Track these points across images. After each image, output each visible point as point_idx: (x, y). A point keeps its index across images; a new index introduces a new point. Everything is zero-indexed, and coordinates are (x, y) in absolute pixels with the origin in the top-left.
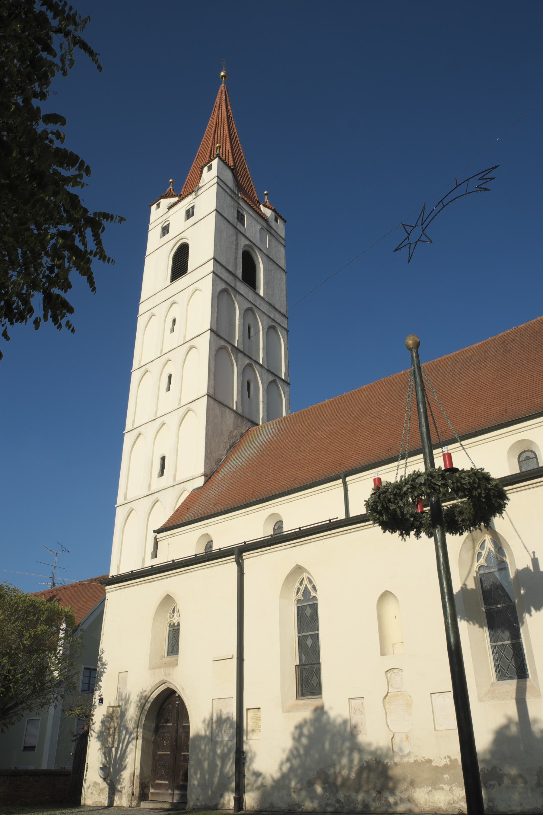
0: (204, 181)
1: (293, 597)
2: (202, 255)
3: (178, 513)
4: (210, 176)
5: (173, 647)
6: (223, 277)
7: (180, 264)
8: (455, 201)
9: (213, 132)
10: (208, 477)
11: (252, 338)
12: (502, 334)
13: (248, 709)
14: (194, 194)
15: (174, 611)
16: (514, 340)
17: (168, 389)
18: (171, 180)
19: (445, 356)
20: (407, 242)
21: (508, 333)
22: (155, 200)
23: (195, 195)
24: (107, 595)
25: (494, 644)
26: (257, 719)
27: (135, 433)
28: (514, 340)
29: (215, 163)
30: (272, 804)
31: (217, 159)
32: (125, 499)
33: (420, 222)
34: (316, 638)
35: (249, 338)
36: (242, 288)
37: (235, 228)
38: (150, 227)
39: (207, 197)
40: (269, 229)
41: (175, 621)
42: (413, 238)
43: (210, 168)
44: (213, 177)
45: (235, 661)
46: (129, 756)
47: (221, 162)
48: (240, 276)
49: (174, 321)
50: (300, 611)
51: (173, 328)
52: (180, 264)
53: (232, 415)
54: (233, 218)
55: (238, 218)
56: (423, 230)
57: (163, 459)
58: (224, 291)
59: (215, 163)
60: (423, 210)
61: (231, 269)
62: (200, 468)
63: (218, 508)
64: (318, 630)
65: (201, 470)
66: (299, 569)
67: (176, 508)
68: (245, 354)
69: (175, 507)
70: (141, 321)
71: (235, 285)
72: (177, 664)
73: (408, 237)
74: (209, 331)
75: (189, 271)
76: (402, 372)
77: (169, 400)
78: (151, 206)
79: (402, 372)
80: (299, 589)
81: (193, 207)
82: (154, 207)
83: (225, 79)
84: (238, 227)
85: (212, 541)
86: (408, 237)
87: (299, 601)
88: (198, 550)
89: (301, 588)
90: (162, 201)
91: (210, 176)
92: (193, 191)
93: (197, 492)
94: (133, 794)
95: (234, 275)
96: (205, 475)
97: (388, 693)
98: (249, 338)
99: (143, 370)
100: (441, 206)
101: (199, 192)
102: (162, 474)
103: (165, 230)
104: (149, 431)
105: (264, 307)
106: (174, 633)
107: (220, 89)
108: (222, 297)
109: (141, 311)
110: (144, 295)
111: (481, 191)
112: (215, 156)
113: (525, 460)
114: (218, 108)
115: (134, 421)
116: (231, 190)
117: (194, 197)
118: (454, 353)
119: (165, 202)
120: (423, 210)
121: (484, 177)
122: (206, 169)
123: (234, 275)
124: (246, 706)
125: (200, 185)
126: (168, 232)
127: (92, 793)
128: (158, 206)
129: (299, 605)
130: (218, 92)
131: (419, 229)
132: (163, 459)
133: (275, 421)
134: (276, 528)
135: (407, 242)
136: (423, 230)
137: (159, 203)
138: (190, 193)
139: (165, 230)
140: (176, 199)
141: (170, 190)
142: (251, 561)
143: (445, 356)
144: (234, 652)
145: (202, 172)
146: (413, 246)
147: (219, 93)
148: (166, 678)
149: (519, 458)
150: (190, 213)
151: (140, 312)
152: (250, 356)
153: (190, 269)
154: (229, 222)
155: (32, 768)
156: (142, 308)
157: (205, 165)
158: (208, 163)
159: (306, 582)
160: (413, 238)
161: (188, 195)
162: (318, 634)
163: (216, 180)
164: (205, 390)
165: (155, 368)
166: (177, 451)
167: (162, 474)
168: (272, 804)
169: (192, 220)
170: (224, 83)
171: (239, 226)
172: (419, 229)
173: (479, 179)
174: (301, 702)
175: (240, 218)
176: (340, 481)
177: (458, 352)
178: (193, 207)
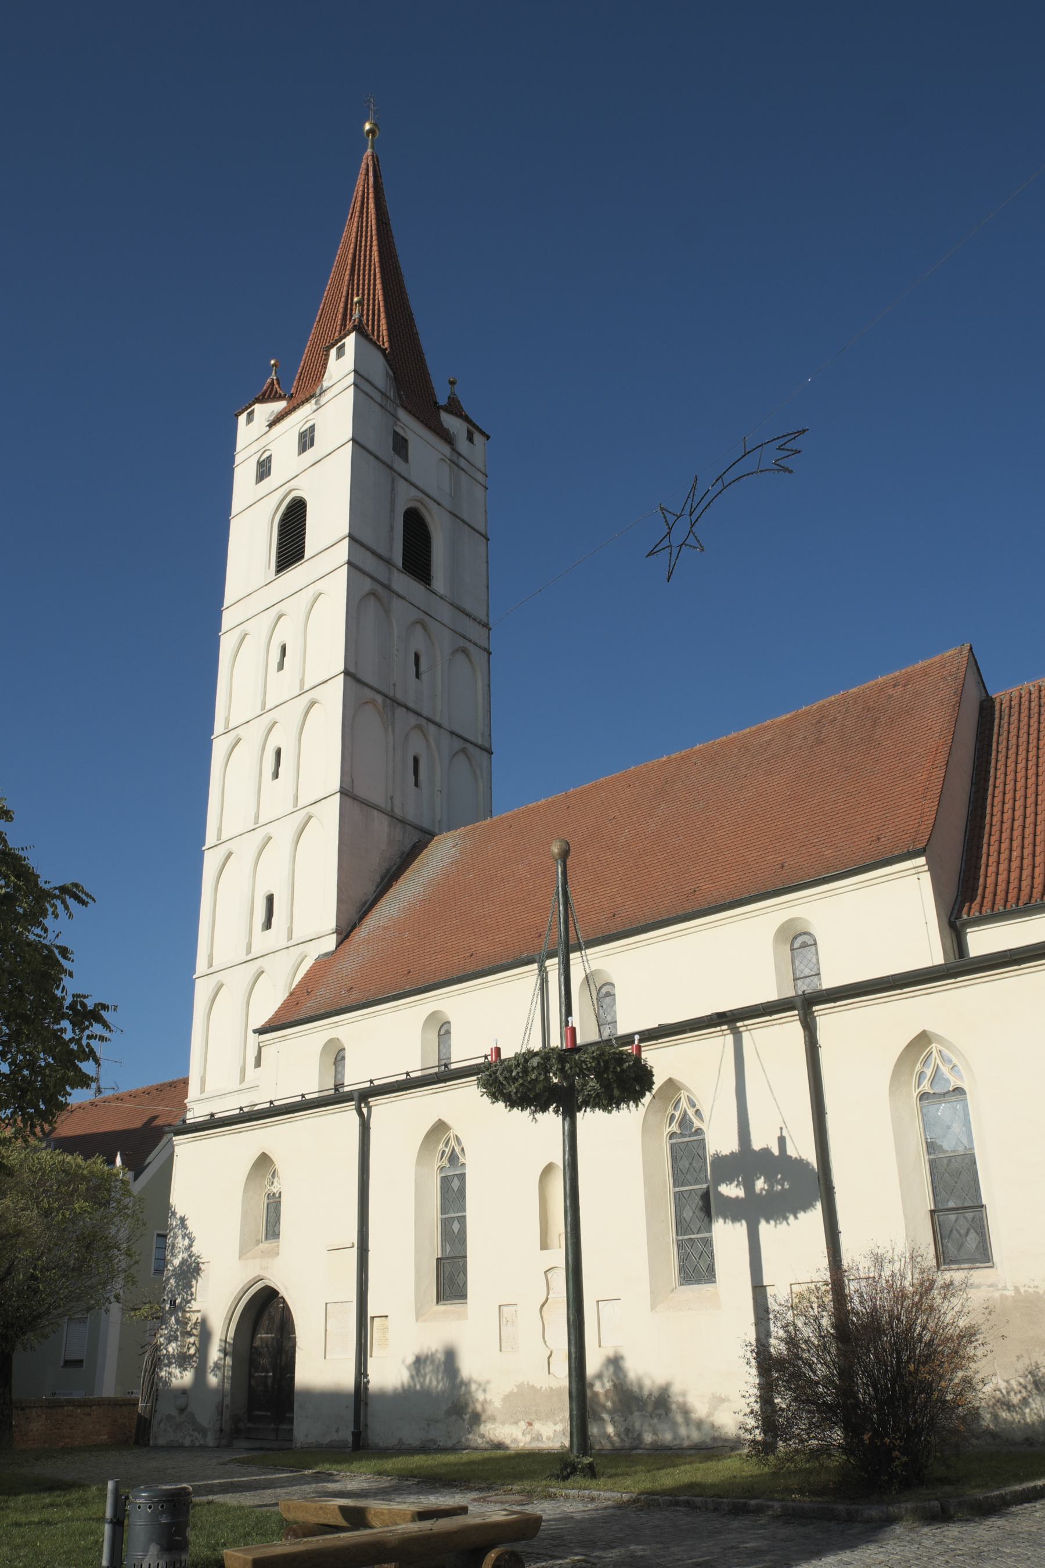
0: (330, 378)
1: (437, 1163)
2: (329, 526)
3: (294, 999)
4: (341, 368)
5: (272, 1229)
6: (367, 568)
7: (290, 545)
8: (741, 480)
9: (350, 261)
10: (345, 932)
11: (424, 677)
12: (821, 702)
13: (373, 1318)
14: (313, 401)
15: (273, 1176)
16: (835, 719)
17: (276, 775)
18: (273, 362)
19: (733, 735)
20: (666, 543)
21: (831, 703)
22: (246, 405)
23: (316, 403)
24: (176, 1148)
25: (680, 1238)
26: (385, 1329)
27: (222, 850)
28: (835, 719)
29: (350, 341)
30: (400, 1439)
31: (353, 335)
32: (210, 965)
33: (687, 511)
34: (462, 1220)
35: (418, 676)
36: (403, 582)
37: (391, 468)
38: (238, 459)
39: (335, 409)
40: (455, 459)
41: (275, 1191)
42: (677, 538)
43: (341, 353)
44: (347, 371)
45: (354, 1252)
46: (891, 1546)
47: (363, 340)
48: (398, 560)
49: (284, 649)
50: (445, 1182)
51: (283, 654)
52: (290, 545)
53: (385, 820)
54: (386, 451)
55: (395, 449)
56: (692, 526)
57: (270, 899)
58: (372, 593)
59: (350, 341)
60: (694, 488)
61: (381, 551)
62: (330, 922)
63: (355, 996)
64: (465, 1211)
65: (332, 924)
66: (440, 1128)
67: (294, 986)
68: (408, 708)
69: (291, 984)
70: (227, 644)
71: (390, 580)
72: (278, 1254)
73: (669, 533)
74: (342, 675)
75: (306, 556)
76: (664, 758)
77: (277, 796)
78: (237, 416)
79: (664, 758)
80: (444, 1152)
81: (312, 428)
82: (242, 418)
83: (373, 136)
84: (395, 466)
85: (344, 1049)
86: (669, 533)
87: (442, 1169)
88: (311, 1083)
89: (447, 1150)
90: (257, 407)
91: (341, 368)
92: (312, 397)
93: (324, 962)
94: (221, 1430)
95: (388, 562)
96: (338, 931)
97: (547, 1299)
98: (418, 676)
99: (232, 736)
100: (719, 485)
101: (323, 400)
102: (268, 925)
103: (264, 469)
104: (245, 850)
105: (445, 613)
106: (274, 1205)
107: (364, 161)
108: (367, 596)
109: (226, 624)
110: (231, 594)
111: (779, 470)
112: (349, 326)
113: (801, 947)
114: (359, 204)
115: (220, 830)
116: (381, 392)
117: (315, 407)
118: (748, 730)
119: (264, 411)
120: (694, 488)
121: (786, 446)
122: (333, 352)
123: (388, 562)
124: (371, 1312)
125: (326, 383)
126: (269, 474)
127: (165, 1430)
128: (250, 418)
129: (443, 1175)
130: (360, 167)
131: (685, 521)
132: (270, 899)
133: (459, 831)
134: (442, 1032)
135: (666, 543)
136: (692, 526)
137: (253, 411)
138: (307, 400)
139: (264, 469)
140: (282, 405)
141: (272, 383)
142: (381, 1109)
143: (733, 735)
144: (353, 1237)
145: (327, 356)
146: (675, 551)
147: (362, 171)
148: (263, 1274)
149: (792, 944)
150: (306, 440)
151: (225, 627)
152: (419, 710)
153: (308, 552)
154: (376, 457)
155: (78, 1395)
156: (228, 619)
157: (333, 345)
158: (336, 341)
159: (453, 1142)
160: (677, 538)
161: (303, 403)
162: (465, 1217)
163: (351, 379)
164: (337, 786)
165: (251, 736)
166: (293, 886)
167: (268, 925)
168: (400, 1439)
169: (311, 454)
170: (373, 148)
171: (398, 464)
172: (685, 521)
173: (779, 449)
174: (441, 1308)
175: (400, 446)
176: (535, 966)
177: (753, 728)
178: (312, 428)
